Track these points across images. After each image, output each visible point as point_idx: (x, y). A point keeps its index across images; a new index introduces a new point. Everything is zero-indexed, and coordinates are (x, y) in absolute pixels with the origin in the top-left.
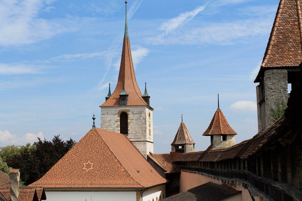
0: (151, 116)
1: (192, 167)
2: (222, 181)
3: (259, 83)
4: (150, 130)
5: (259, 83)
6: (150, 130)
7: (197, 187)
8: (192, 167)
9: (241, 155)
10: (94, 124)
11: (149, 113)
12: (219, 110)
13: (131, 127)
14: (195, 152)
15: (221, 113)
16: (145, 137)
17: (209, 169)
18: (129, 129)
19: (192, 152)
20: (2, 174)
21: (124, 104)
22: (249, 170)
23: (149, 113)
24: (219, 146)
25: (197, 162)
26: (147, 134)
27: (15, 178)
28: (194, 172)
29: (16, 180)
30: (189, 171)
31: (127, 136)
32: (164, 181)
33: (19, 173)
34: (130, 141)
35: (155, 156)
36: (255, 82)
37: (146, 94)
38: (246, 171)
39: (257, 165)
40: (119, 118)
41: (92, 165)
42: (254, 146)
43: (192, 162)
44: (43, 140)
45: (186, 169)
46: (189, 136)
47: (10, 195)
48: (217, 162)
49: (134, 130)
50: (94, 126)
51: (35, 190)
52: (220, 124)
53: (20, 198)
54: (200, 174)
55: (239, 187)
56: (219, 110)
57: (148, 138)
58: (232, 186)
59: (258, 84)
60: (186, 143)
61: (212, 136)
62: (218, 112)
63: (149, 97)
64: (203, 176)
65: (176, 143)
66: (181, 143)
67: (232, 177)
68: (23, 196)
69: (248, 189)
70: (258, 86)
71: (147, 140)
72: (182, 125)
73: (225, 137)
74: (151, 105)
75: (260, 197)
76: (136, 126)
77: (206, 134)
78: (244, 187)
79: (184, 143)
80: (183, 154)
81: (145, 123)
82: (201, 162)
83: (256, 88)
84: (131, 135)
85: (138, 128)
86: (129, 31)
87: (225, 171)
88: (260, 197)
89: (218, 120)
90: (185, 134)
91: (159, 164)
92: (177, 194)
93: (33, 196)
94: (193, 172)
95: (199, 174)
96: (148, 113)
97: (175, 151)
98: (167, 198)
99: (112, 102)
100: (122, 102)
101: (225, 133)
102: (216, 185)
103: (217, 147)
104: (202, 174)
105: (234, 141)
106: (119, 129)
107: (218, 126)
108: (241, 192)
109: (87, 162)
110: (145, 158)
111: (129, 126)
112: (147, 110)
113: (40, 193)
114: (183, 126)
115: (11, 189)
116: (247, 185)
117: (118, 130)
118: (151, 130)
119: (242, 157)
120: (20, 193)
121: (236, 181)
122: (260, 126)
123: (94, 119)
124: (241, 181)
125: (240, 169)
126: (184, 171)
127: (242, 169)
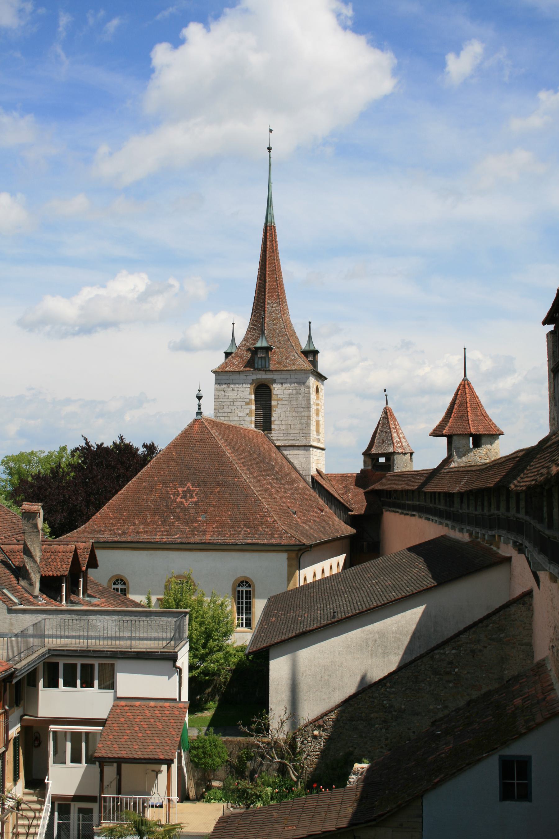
0: (321, 393)
1: (407, 502)
2: (471, 535)
3: (554, 325)
4: (318, 423)
5: (554, 325)
6: (318, 423)
7: (416, 546)
8: (407, 502)
9: (511, 482)
10: (199, 409)
11: (317, 386)
12: (466, 382)
13: (279, 416)
14: (414, 469)
15: (471, 389)
16: (308, 437)
17: (442, 507)
18: (273, 419)
19: (407, 469)
20: (7, 512)
21: (267, 360)
22: (527, 513)
23: (317, 386)
24: (465, 459)
25: (419, 492)
26: (311, 432)
27: (365, 761)
28: (410, 513)
29: (36, 526)
30: (400, 511)
31: (269, 435)
32: (349, 530)
33: (42, 512)
34: (276, 446)
35: (329, 478)
36: (544, 323)
37: (311, 344)
38: (522, 515)
39: (545, 503)
40: (253, 397)
41: (191, 487)
42: (540, 463)
43: (407, 491)
44: (94, 444)
45: (394, 507)
46: (401, 436)
47: (22, 557)
48: (461, 495)
49: (284, 422)
50: (199, 413)
51: (74, 547)
52: (467, 412)
53: (43, 563)
54: (423, 518)
55: (506, 550)
56: (466, 382)
57: (314, 441)
58: (492, 547)
59: (551, 327)
60: (394, 452)
61: (450, 438)
62: (464, 386)
63: (317, 352)
64: (431, 522)
65: (374, 451)
66: (385, 451)
67: (491, 528)
68: (50, 560)
69: (525, 554)
70: (551, 332)
71: (313, 443)
72: (386, 413)
73: (478, 440)
74: (321, 369)
75: (550, 573)
76: (288, 412)
77: (437, 433)
78: (517, 549)
79: (390, 450)
80: (389, 474)
81: (308, 407)
82: (425, 493)
83: (547, 336)
84: (278, 435)
85: (292, 418)
86: (276, 211)
87: (476, 513)
88: (550, 573)
89: (463, 404)
90: (393, 431)
91: (337, 496)
92: (374, 560)
93: (70, 560)
94: (408, 512)
95: (420, 517)
96: (315, 388)
97: (370, 468)
98: (353, 568)
99: (239, 362)
100: (260, 363)
101: (479, 431)
102: (457, 542)
103: (457, 463)
104: (428, 519)
105: (502, 448)
106: (253, 419)
107: (461, 417)
108: (508, 560)
109: (186, 485)
110: (307, 483)
111: (274, 414)
112: (312, 381)
113: (85, 553)
114: (389, 414)
115: (25, 545)
116: (524, 547)
117: (251, 423)
118: (321, 422)
119: (512, 486)
120: (45, 554)
121: (500, 536)
122: (554, 419)
123: (199, 398)
124: (509, 537)
125: (508, 510)
126: (389, 511)
127: (513, 511)
